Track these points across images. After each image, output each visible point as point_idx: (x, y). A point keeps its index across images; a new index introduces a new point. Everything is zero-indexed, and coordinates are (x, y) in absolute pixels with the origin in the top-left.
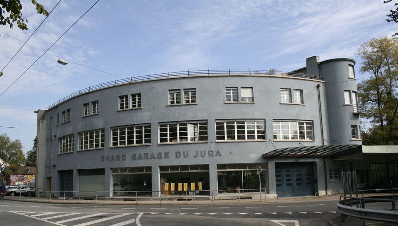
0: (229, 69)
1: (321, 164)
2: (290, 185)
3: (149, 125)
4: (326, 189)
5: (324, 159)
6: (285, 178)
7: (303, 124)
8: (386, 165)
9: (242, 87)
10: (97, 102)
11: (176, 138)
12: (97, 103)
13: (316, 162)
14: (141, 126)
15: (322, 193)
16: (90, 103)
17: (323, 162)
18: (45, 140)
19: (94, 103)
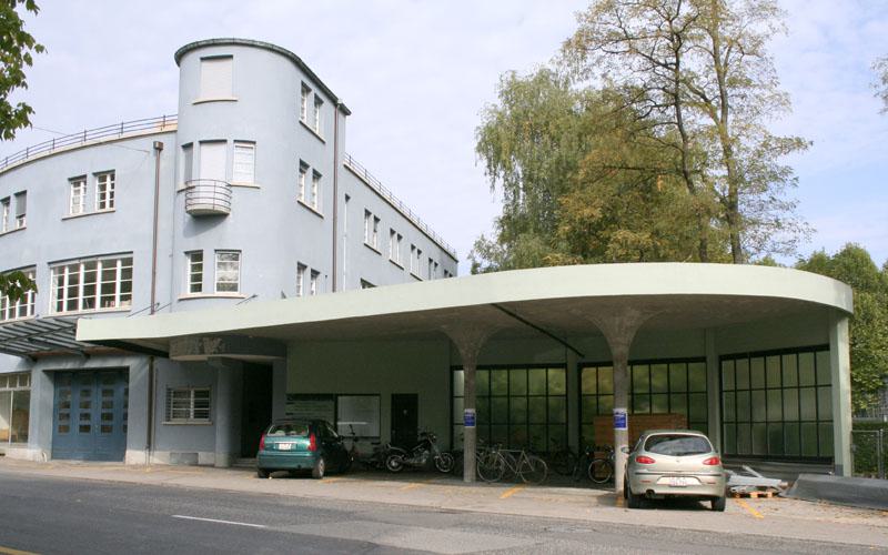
0: (120, 122)
1: (139, 377)
2: (85, 429)
3: (129, 256)
4: (149, 446)
5: (152, 359)
6: (76, 411)
7: (113, 263)
8: (341, 395)
9: (201, 142)
10: (24, 193)
11: (113, 298)
12: (113, 179)
13: (127, 369)
14: (77, 262)
15: (135, 456)
16: (90, 178)
17: (148, 367)
18: (456, 342)
19: (101, 176)
